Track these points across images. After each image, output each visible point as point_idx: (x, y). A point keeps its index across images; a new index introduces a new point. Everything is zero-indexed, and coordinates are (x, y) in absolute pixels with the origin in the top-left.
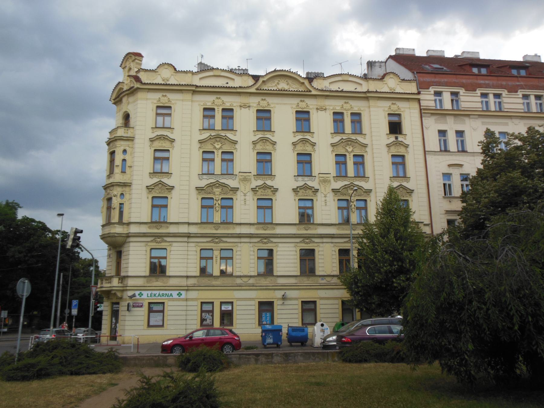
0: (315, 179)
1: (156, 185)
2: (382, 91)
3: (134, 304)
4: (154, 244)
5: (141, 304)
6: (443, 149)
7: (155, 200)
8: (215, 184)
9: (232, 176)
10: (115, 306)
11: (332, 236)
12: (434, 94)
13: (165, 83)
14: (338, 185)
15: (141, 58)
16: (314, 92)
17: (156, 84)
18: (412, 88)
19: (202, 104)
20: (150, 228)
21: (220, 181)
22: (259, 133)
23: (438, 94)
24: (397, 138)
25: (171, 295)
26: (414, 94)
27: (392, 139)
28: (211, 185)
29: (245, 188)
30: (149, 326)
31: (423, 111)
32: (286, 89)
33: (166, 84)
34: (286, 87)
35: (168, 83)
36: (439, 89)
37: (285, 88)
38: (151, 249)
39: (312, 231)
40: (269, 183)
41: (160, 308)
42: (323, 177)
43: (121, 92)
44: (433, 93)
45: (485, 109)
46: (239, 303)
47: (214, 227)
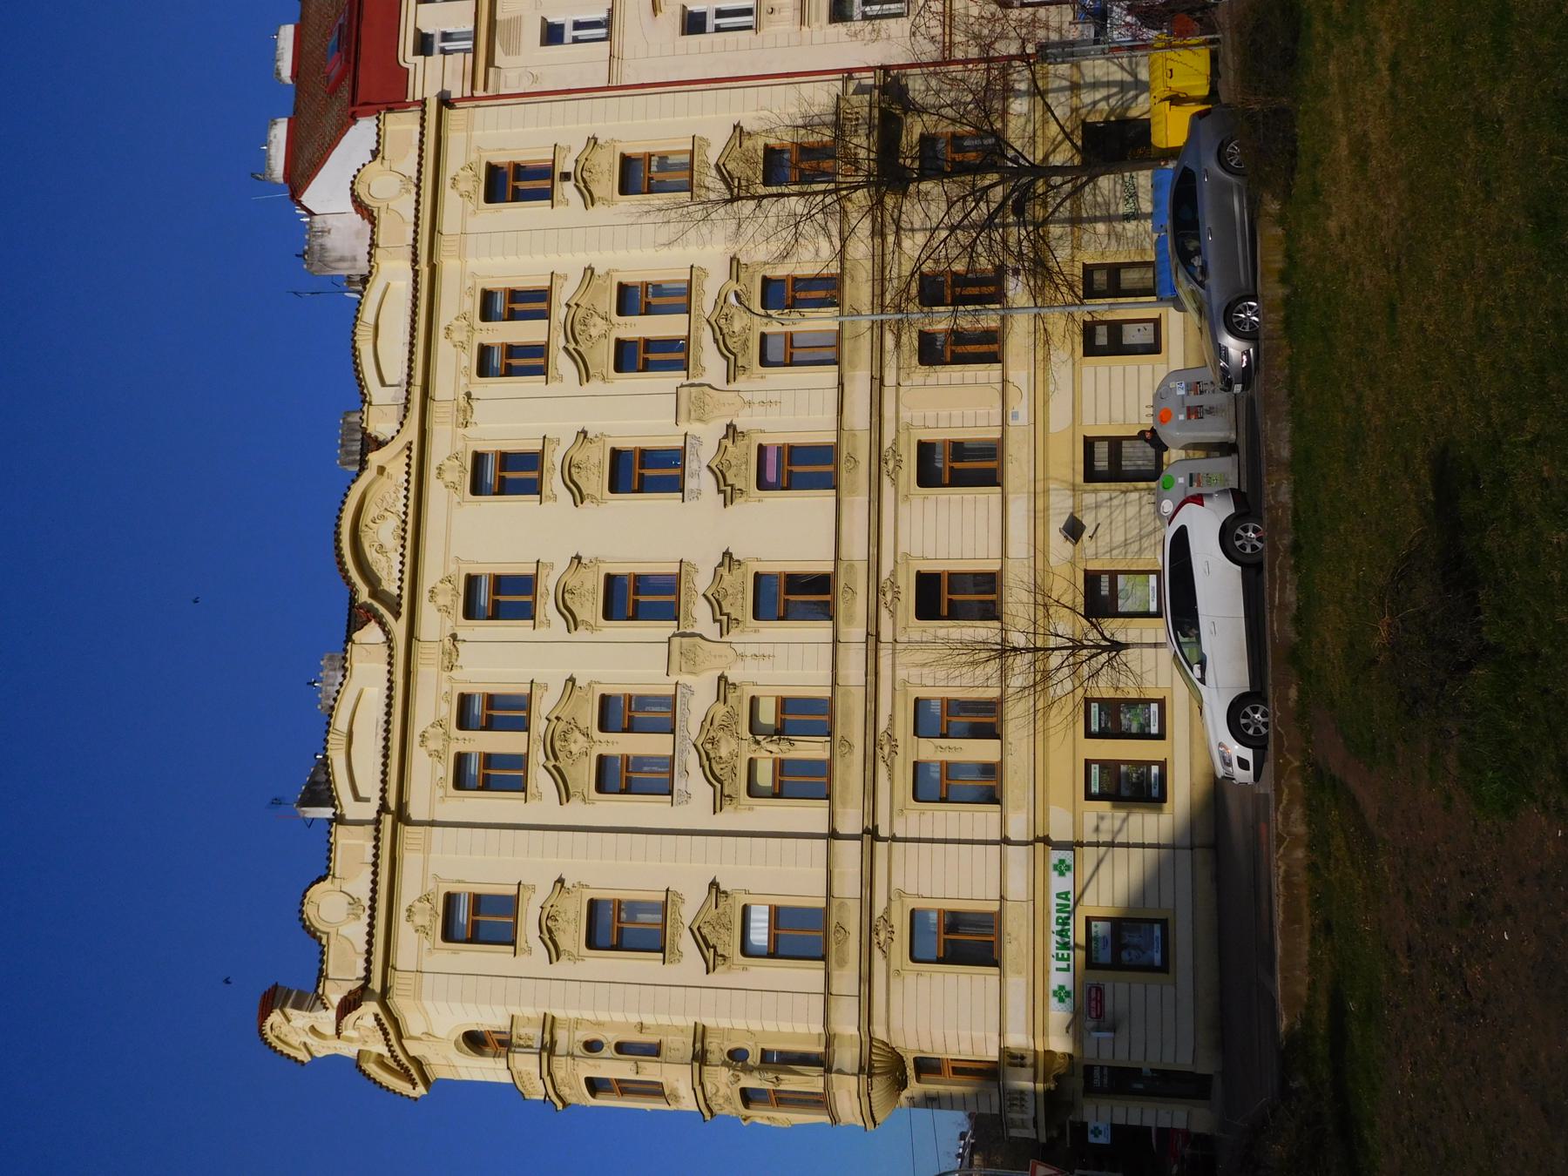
0: (694, 437)
1: (704, 944)
2: (413, 219)
3: (1094, 1014)
4: (895, 947)
5: (1094, 990)
6: (601, 32)
7: (771, 357)
8: (717, 328)
9: (696, 154)
10: (1097, 1082)
11: (878, 382)
12: (426, 55)
13: (368, 912)
14: (711, 363)
15: (278, 994)
16: (412, 432)
17: (370, 943)
18: (402, 126)
19: (440, 792)
20: (842, 963)
21: (693, 737)
22: (542, 610)
23: (424, 45)
24: (566, 176)
25: (1063, 895)
26: (423, 119)
27: (567, 190)
28: (720, 338)
29: (721, 656)
30: (1164, 968)
31: (479, 93)
32: (399, 523)
33: (373, 908)
34: (393, 522)
35: (367, 903)
36: (407, 42)
37: (395, 525)
38: (913, 959)
39: (861, 448)
40: (703, 581)
41: (1102, 450)
42: (690, 411)
43: (394, 1065)
44: (423, 57)
45: (469, 44)
46: (1088, 419)
47: (843, 756)
